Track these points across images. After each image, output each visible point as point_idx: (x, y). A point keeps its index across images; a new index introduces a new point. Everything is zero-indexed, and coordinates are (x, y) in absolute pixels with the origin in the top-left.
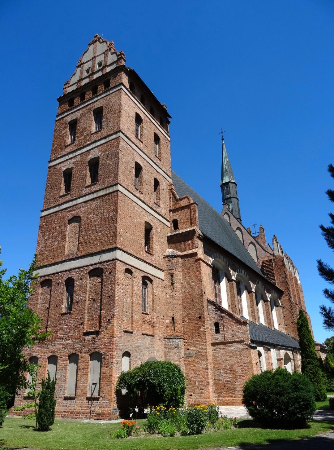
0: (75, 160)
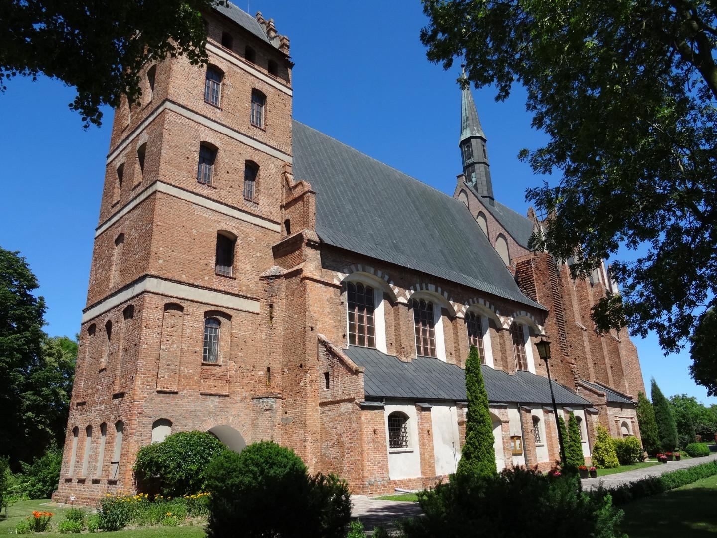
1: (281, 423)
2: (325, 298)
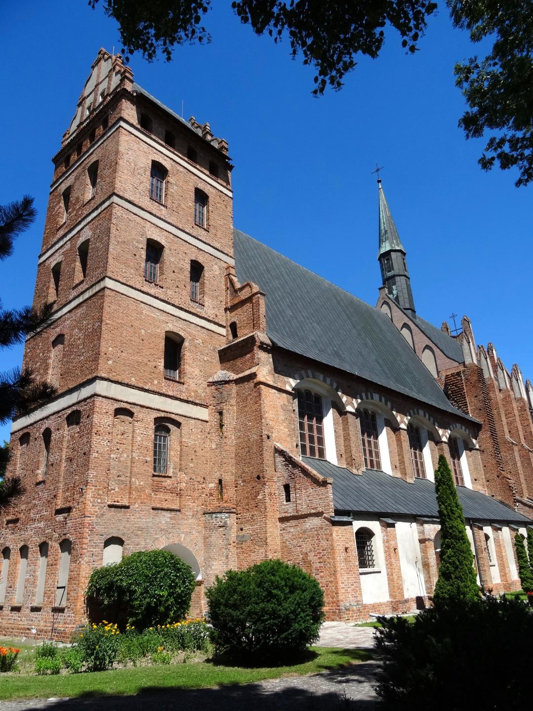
0: (65, 249)
1: (236, 541)
2: (279, 405)
